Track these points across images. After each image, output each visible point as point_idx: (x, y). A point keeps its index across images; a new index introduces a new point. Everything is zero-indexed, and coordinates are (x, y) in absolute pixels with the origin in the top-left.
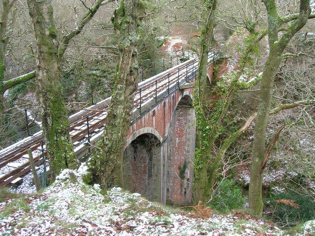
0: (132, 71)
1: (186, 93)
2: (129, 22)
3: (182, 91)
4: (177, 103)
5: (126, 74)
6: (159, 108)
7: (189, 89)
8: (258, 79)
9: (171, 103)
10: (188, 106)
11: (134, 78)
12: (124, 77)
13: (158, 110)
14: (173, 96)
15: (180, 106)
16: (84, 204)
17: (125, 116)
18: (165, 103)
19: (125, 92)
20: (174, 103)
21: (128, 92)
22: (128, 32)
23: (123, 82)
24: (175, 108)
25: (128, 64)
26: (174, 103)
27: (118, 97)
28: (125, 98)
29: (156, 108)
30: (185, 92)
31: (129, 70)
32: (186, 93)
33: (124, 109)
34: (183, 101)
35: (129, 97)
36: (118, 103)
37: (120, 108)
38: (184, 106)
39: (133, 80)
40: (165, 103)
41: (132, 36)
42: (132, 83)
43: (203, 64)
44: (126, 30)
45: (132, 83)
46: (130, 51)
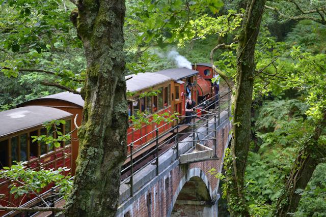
0: (116, 121)
1: (194, 172)
2: (110, 23)
3: (185, 167)
4: (176, 195)
5: (104, 127)
6: (138, 207)
7: (200, 164)
8: (272, 69)
9: (162, 195)
10: (198, 203)
11: (119, 134)
12: (100, 131)
13: (136, 212)
14: (167, 179)
15: (182, 203)
16: (288, 159)
17: (102, 212)
18: (149, 195)
19: (102, 162)
20: (170, 196)
21: (108, 163)
22: (109, 43)
23: (98, 143)
24: (172, 206)
25: (110, 106)
26: (170, 196)
27: (89, 174)
28: (103, 174)
29: (131, 207)
30: (191, 171)
31: (109, 117)
32: (194, 172)
33: (100, 197)
34: (188, 191)
35: (111, 173)
36: (89, 186)
37: (93, 195)
38: (190, 202)
39: (118, 138)
40: (149, 195)
41: (116, 50)
42: (116, 146)
43: (242, 105)
44: (105, 40)
45: (116, 146)
46: (113, 81)
